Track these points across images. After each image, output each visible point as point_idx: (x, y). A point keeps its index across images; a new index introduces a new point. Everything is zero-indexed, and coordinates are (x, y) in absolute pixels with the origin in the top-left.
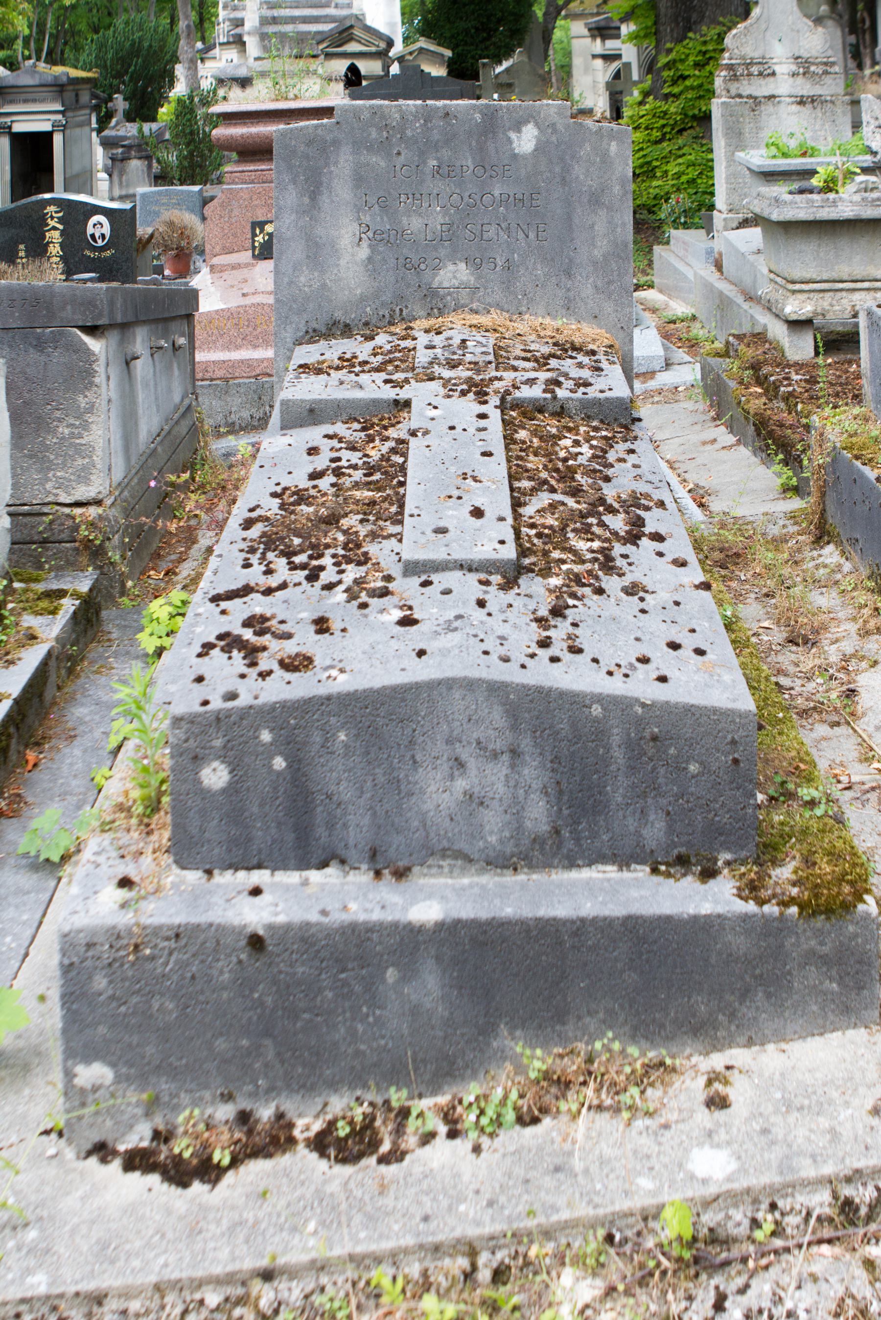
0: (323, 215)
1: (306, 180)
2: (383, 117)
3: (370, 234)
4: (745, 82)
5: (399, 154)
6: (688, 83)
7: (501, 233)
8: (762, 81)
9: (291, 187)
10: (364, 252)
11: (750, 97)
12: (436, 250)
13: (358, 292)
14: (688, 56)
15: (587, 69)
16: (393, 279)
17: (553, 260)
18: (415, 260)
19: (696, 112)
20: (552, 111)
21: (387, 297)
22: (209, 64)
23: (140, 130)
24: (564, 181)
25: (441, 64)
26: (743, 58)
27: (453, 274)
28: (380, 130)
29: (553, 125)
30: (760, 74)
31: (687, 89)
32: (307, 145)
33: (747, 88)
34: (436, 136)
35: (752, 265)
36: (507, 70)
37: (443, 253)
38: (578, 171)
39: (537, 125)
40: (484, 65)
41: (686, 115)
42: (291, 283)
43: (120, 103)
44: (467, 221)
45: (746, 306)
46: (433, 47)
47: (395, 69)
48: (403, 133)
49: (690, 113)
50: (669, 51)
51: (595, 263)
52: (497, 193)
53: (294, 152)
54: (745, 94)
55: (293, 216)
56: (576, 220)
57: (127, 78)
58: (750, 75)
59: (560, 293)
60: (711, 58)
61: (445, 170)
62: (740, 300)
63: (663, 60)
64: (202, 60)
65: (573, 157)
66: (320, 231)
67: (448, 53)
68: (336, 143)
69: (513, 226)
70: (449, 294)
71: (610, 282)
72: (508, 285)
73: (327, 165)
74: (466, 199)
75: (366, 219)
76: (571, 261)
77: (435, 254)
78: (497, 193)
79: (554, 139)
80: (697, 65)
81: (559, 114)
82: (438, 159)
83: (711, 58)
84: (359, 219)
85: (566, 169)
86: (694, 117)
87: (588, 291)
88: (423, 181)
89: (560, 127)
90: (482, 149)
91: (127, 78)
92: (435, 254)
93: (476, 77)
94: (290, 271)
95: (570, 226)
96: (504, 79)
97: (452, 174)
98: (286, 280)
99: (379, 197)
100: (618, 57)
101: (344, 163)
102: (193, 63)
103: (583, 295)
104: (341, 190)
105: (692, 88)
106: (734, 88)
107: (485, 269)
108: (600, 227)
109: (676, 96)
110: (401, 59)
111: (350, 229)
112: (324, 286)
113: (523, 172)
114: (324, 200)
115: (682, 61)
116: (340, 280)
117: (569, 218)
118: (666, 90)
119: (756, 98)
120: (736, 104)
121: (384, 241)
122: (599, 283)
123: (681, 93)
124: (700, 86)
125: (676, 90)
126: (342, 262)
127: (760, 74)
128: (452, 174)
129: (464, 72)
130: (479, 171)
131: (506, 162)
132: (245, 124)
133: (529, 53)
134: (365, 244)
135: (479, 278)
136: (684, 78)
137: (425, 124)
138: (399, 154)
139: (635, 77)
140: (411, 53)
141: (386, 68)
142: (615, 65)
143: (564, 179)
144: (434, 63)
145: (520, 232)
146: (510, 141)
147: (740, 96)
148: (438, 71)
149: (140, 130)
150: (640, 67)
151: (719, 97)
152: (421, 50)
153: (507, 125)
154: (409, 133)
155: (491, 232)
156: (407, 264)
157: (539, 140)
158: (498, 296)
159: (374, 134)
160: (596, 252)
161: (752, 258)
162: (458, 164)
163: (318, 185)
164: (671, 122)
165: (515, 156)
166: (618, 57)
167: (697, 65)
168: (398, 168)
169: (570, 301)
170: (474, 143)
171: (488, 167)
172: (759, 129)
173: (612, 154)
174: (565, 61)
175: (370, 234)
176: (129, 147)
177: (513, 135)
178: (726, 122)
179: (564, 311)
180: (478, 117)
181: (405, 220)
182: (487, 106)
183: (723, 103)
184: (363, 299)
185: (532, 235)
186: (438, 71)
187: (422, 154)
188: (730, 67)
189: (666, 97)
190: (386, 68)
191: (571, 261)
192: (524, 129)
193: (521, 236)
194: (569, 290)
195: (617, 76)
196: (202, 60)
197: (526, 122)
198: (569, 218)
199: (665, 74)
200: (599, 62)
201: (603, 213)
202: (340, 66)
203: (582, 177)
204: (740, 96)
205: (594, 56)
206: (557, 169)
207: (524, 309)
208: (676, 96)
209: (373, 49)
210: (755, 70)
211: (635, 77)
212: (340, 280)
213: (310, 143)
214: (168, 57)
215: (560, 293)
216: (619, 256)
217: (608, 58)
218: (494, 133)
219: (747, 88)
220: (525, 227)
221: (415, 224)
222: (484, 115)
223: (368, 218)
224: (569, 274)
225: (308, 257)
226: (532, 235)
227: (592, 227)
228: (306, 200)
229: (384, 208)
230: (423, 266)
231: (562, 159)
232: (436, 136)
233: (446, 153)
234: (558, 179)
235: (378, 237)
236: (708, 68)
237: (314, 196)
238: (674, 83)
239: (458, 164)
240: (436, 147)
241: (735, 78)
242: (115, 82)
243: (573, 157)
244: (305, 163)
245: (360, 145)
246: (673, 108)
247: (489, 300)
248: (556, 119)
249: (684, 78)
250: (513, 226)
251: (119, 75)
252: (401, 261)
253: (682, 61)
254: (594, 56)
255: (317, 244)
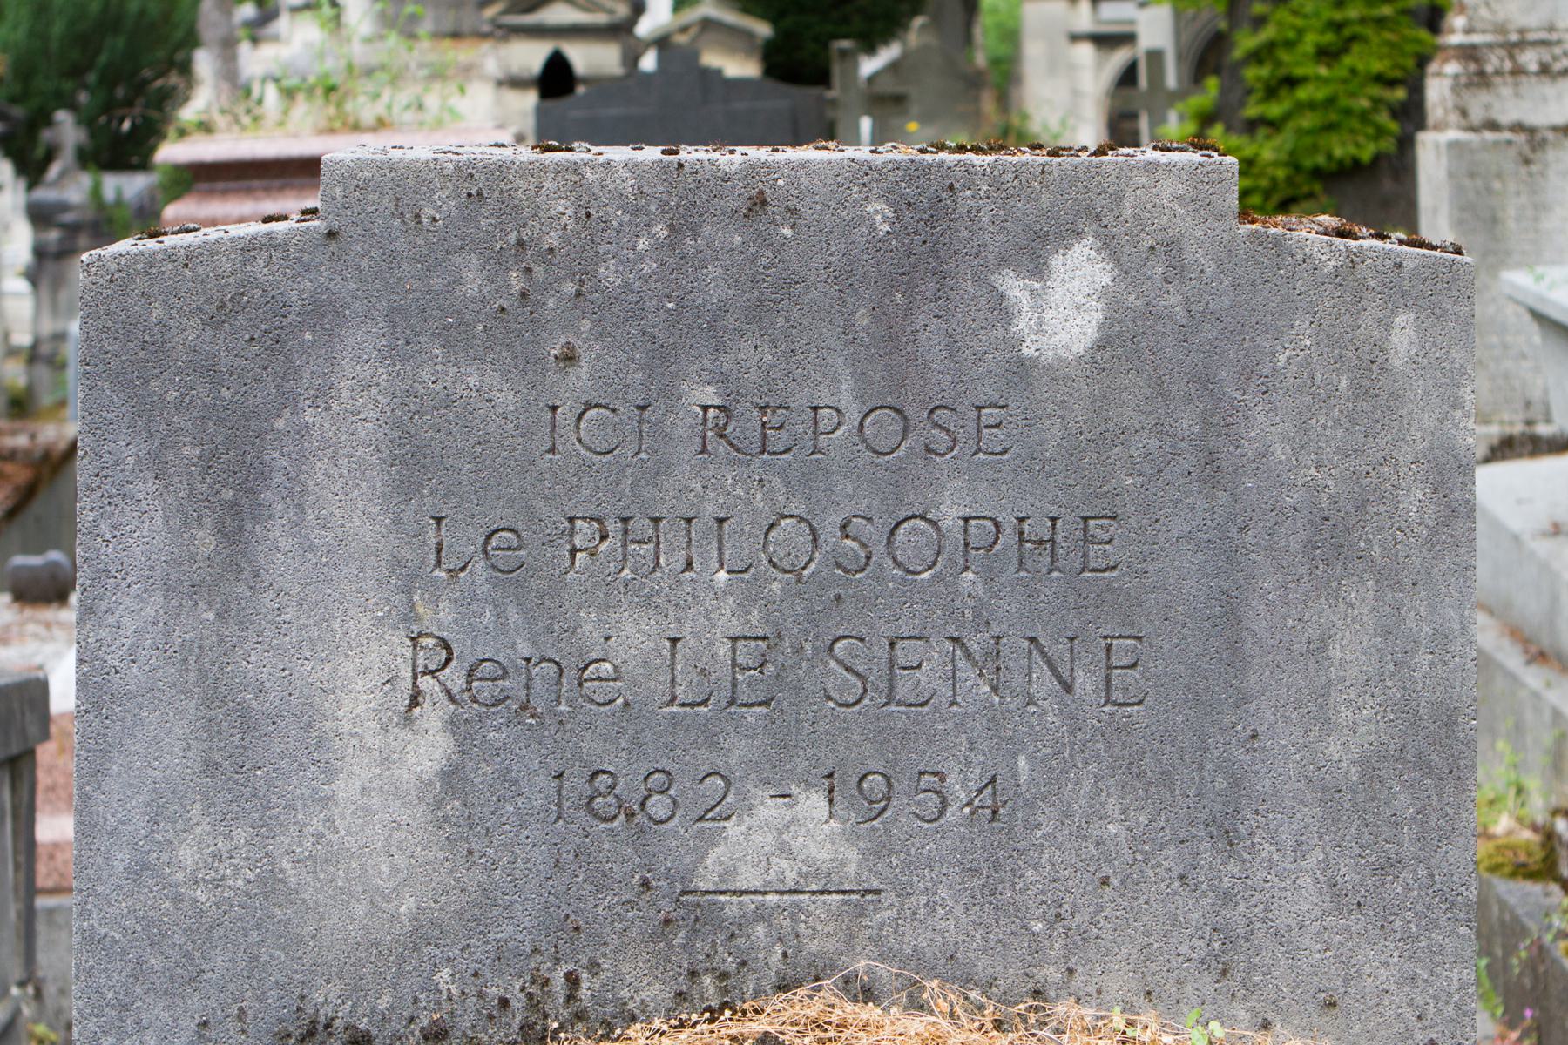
0: (268, 601)
1: (207, 463)
2: (509, 211)
3: (454, 677)
4: (1506, 91)
5: (569, 357)
6: (1302, 93)
7: (967, 673)
8: (1548, 89)
9: (145, 487)
10: (429, 748)
11: (1518, 127)
12: (711, 740)
13: (407, 906)
14: (1300, 32)
15: (1053, 65)
16: (540, 855)
17: (1167, 780)
18: (630, 785)
19: (1320, 160)
20: (1169, 188)
21: (517, 927)
22: (267, 51)
23: (96, 192)
24: (1211, 470)
25: (748, 52)
26: (1501, 29)
27: (779, 839)
28: (496, 261)
29: (1171, 247)
30: (1545, 70)
31: (1301, 107)
32: (212, 322)
33: (1510, 105)
34: (714, 287)
35: (1545, 567)
36: (893, 67)
37: (737, 751)
38: (1267, 428)
39: (1109, 246)
40: (844, 53)
41: (1297, 168)
42: (139, 870)
43: (67, 130)
44: (832, 627)
45: (1533, 678)
46: (731, 17)
47: (648, 62)
48: (585, 277)
49: (1308, 163)
50: (1259, 22)
51: (1330, 793)
52: (950, 513)
53: (159, 348)
54: (1505, 119)
55: (154, 606)
56: (1258, 623)
57: (92, 78)
58: (1518, 71)
59: (1196, 911)
60: (1354, 38)
61: (747, 425)
62: (1512, 658)
63: (1246, 42)
64: (255, 41)
65: (1246, 373)
66: (256, 665)
67: (763, 29)
68: (323, 314)
69: (1016, 644)
70: (761, 915)
71: (1386, 867)
72: (990, 881)
73: (288, 400)
74: (830, 536)
75: (440, 616)
76: (1236, 782)
77: (707, 758)
78: (950, 513)
79: (1173, 300)
80: (1325, 54)
81: (1196, 203)
82: (721, 379)
83: (1354, 38)
84: (410, 615)
85: (1222, 421)
86: (1317, 173)
87: (1302, 900)
88: (662, 468)
89: (1197, 254)
90: (893, 341)
91: (92, 78)
92: (707, 758)
93: (822, 78)
94: (140, 823)
95: (1235, 645)
96: (888, 86)
97: (778, 440)
98: (122, 857)
99: (486, 527)
100: (1128, 39)
101: (353, 398)
102: (228, 46)
103: (1283, 919)
104: (341, 499)
105: (1312, 105)
106: (1478, 105)
107: (903, 818)
108: (1352, 652)
109: (1274, 125)
110: (662, 42)
111: (374, 656)
112: (270, 883)
113: (1054, 430)
114: (276, 537)
115: (1289, 45)
116: (333, 858)
117: (1229, 612)
118: (1252, 111)
119: (1531, 131)
120: (1485, 146)
121: (504, 702)
122: (1346, 872)
123: (1287, 117)
124: (1330, 102)
125: (1275, 110)
126: (345, 789)
127: (1545, 70)
128: (778, 440)
129: (798, 64)
130: (884, 427)
131: (988, 392)
132: (249, 192)
133: (937, 22)
134: (432, 716)
135: (878, 851)
136: (1292, 82)
137: (673, 241)
138: (569, 357)
139: (1171, 80)
140: (684, 29)
141: (631, 59)
142: (1120, 57)
143: (1211, 460)
144: (731, 50)
145: (1041, 670)
146: (1001, 309)
147: (1493, 126)
148: (739, 67)
149: (96, 192)
150: (1180, 57)
151: (1438, 127)
152: (707, 24)
153: (994, 245)
154: (609, 275)
155: (929, 669)
156: (596, 798)
157: (1114, 308)
158: (948, 922)
159: (473, 282)
160: (1333, 750)
161: (1542, 547)
162: (800, 400)
163: (251, 480)
164: (1264, 183)
165: (1021, 370)
166: (1128, 39)
167: (1325, 54)
168: (565, 416)
169: (1230, 941)
170: (863, 319)
171: (915, 413)
172: (1541, 208)
173: (1397, 362)
174: (1003, 50)
175: (454, 677)
176: (73, 229)
177: (1014, 287)
178: (1458, 190)
179: (1207, 983)
180: (878, 210)
181: (589, 625)
182: (915, 171)
183: (1454, 145)
184: (423, 933)
185: (1086, 684)
186: (739, 67)
187: (660, 357)
188: (1469, 53)
189: (1251, 126)
190: (631, 59)
191: (1236, 782)
192: (1057, 262)
193: (1042, 683)
194: (1227, 898)
195: (1128, 76)
196: (255, 41)
197: (1068, 234)
198: (1230, 612)
199: (1251, 73)
200: (1086, 51)
201: (1361, 593)
202: (531, 56)
203: (1280, 452)
204: (1493, 126)
205: (1075, 38)
206: (1187, 423)
207: (1052, 974)
208: (1274, 125)
209: (600, 18)
210: (1530, 59)
211: (1171, 80)
212: (333, 858)
213: (220, 314)
214: (179, 34)
215: (1196, 911)
216: (1422, 764)
217: (1105, 41)
218: (941, 276)
219: (1510, 105)
220: (1058, 650)
221: (629, 638)
222: (902, 206)
223: (447, 614)
224: (1227, 838)
225: (210, 766)
226: (1086, 684)
227: (1318, 649)
228: (205, 540)
229: (508, 573)
230: (659, 806)
231: (1205, 382)
232: (714, 287)
233: (750, 357)
234: (1188, 461)
235: (486, 690)
236: (1348, 60)
237: (236, 521)
238: (1271, 92)
239: (800, 400)
240: (715, 333)
241: (1481, 80)
242: (68, 85)
243: (1246, 373)
244: (201, 393)
245: (415, 322)
246: (1268, 150)
247: (917, 939)
248: (1182, 221)
249: (1292, 82)
250: (1016, 644)
251: (76, 73)
252: (576, 782)
253: (1289, 45)
254: (1075, 38)
255: (244, 715)
